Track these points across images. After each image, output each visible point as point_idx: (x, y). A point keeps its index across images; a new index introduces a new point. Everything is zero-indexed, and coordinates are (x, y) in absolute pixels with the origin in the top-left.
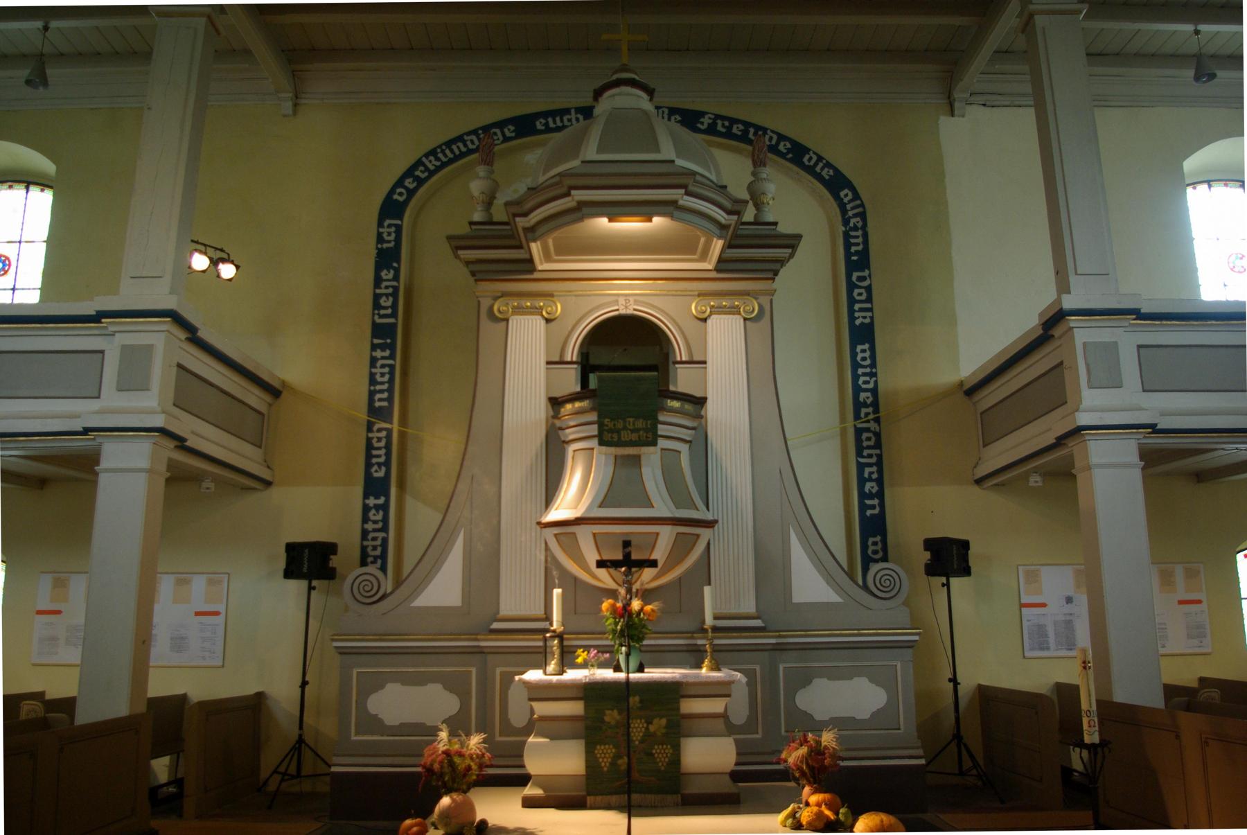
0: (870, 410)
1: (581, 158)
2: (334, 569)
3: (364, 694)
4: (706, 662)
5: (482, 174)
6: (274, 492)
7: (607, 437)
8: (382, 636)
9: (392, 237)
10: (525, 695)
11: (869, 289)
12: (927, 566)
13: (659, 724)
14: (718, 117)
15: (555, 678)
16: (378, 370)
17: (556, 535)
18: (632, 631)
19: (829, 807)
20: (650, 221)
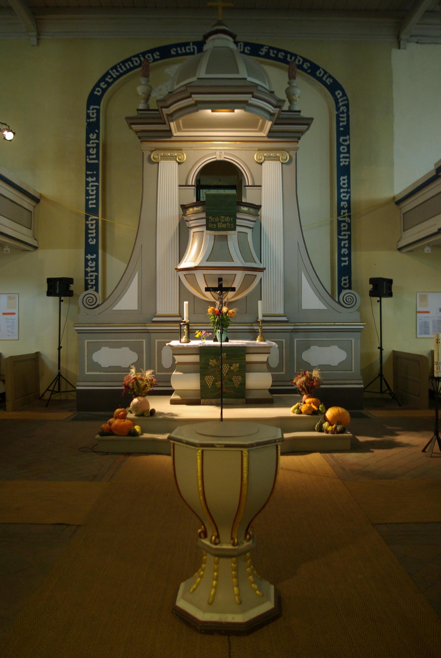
0: (346, 211)
1: (197, 76)
2: (72, 291)
3: (90, 354)
4: (259, 337)
5: (143, 82)
6: (39, 252)
7: (211, 225)
8: (98, 325)
9: (95, 115)
10: (171, 352)
11: (348, 146)
12: (370, 291)
13: (235, 366)
14: (271, 48)
15: (185, 345)
16: (90, 188)
17: (185, 275)
18: (222, 322)
19: (315, 404)
20: (234, 111)
